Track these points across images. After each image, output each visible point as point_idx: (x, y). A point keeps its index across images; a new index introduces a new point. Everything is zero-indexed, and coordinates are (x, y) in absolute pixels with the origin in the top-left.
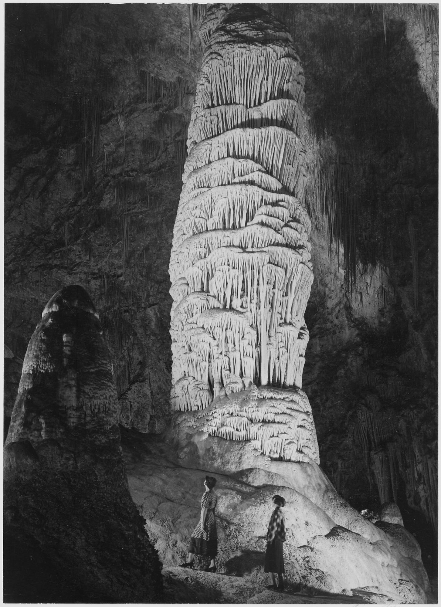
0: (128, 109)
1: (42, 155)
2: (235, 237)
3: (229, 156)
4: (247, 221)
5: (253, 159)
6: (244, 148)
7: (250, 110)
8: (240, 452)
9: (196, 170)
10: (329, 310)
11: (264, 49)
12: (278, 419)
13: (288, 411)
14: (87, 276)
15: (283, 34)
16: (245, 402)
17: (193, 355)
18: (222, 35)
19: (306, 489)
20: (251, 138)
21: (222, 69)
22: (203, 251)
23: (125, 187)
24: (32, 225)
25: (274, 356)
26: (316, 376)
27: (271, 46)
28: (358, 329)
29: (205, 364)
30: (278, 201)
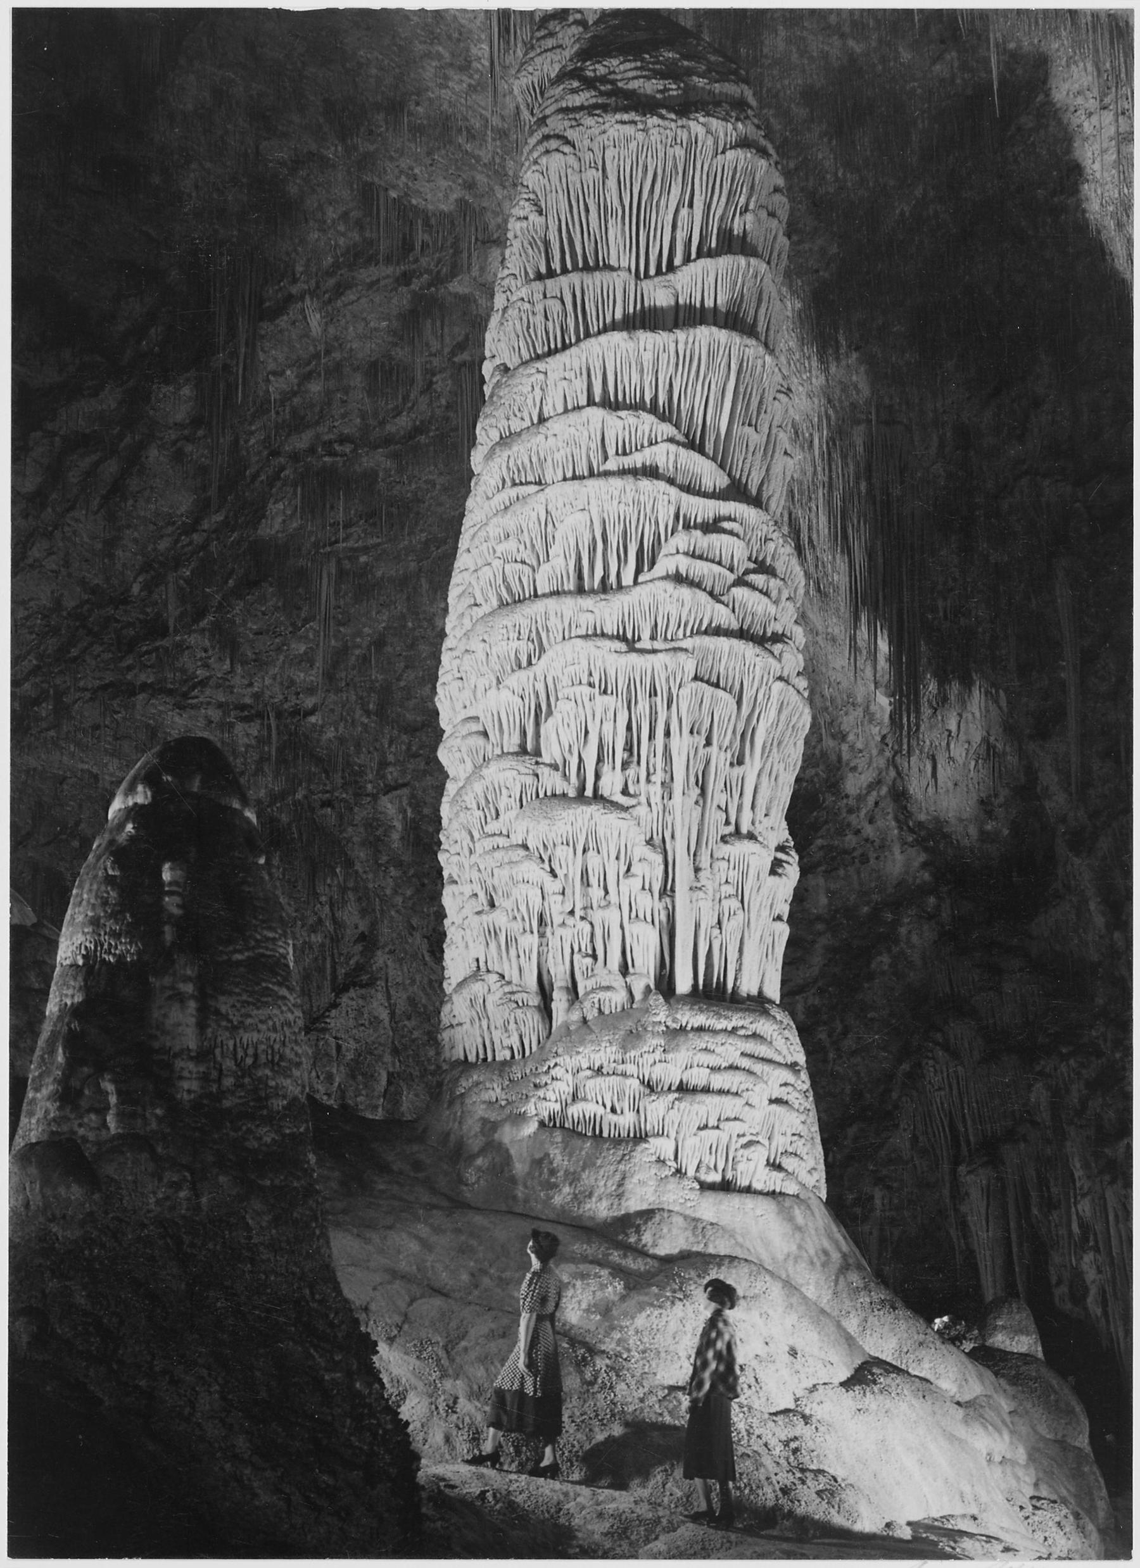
0: (332, 282)
1: (110, 400)
2: (608, 612)
3: (591, 402)
4: (638, 571)
5: (653, 409)
6: (632, 383)
7: (646, 285)
8: (622, 1167)
9: (507, 439)
10: (851, 802)
11: (683, 127)
12: (718, 1081)
13: (745, 1063)
14: (226, 714)
15: (731, 89)
16: (633, 1037)
17: (499, 918)
18: (574, 91)
19: (791, 1262)
20: (647, 357)
21: (574, 178)
22: (524, 647)
23: (323, 484)
24: (83, 582)
25: (708, 921)
26: (816, 971)
27: (702, 119)
28: (926, 849)
29: (530, 941)
30: (718, 519)
